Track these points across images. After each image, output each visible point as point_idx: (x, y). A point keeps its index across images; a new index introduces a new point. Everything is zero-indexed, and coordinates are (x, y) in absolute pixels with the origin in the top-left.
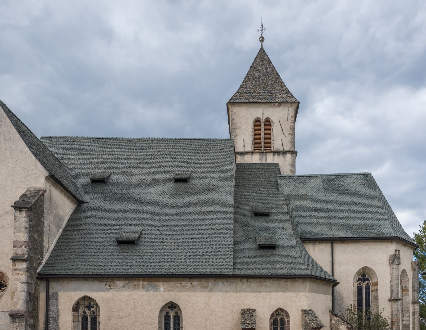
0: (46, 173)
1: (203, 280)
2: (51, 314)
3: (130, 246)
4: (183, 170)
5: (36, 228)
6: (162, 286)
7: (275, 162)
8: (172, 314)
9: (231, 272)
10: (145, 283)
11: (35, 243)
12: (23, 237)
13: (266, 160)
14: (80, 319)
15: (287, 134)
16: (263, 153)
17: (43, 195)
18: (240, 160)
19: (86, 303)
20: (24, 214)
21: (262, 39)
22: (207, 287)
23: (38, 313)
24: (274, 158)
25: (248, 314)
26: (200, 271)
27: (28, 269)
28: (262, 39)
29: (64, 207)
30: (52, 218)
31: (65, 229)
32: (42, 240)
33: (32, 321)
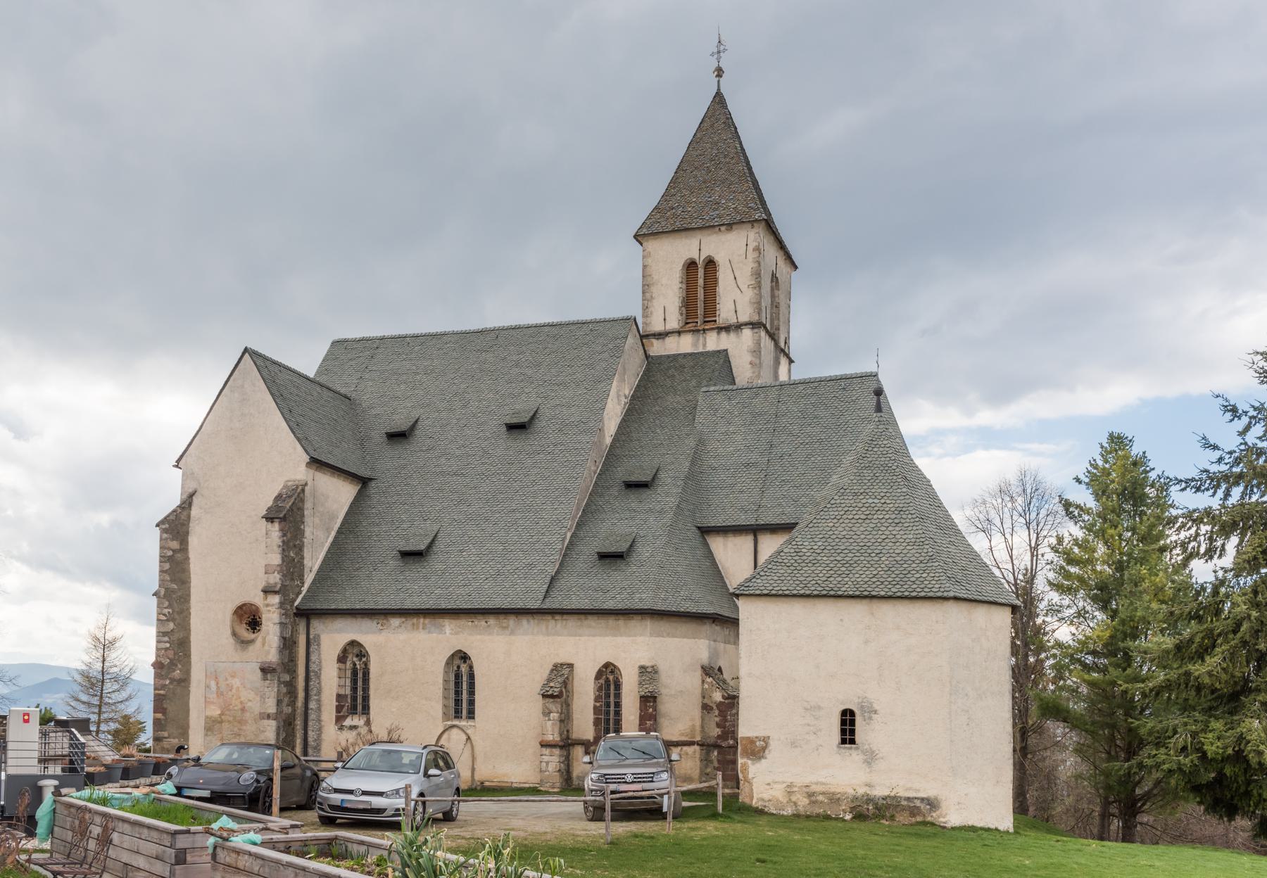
0: (307, 459)
1: (502, 617)
2: (313, 667)
3: (417, 558)
4: (520, 409)
5: (292, 544)
6: (448, 625)
7: (722, 347)
8: (464, 668)
9: (536, 605)
10: (427, 621)
11: (292, 565)
12: (276, 559)
13: (704, 345)
14: (349, 673)
15: (744, 288)
16: (698, 331)
17: (303, 491)
18: (657, 348)
19: (356, 651)
20: (276, 526)
21: (719, 72)
22: (507, 628)
23: (296, 665)
24: (718, 339)
25: (562, 674)
26: (498, 603)
27: (282, 604)
28: (719, 72)
29: (336, 496)
30: (317, 520)
31: (340, 532)
32: (303, 558)
33: (287, 678)
